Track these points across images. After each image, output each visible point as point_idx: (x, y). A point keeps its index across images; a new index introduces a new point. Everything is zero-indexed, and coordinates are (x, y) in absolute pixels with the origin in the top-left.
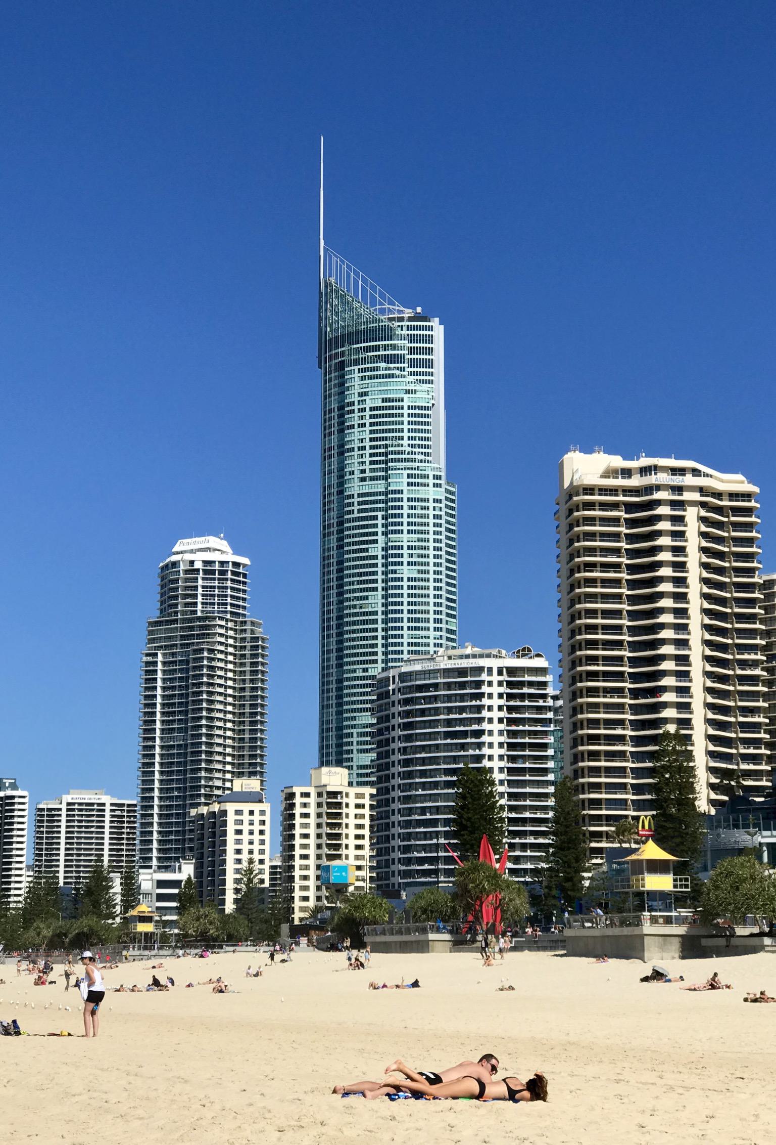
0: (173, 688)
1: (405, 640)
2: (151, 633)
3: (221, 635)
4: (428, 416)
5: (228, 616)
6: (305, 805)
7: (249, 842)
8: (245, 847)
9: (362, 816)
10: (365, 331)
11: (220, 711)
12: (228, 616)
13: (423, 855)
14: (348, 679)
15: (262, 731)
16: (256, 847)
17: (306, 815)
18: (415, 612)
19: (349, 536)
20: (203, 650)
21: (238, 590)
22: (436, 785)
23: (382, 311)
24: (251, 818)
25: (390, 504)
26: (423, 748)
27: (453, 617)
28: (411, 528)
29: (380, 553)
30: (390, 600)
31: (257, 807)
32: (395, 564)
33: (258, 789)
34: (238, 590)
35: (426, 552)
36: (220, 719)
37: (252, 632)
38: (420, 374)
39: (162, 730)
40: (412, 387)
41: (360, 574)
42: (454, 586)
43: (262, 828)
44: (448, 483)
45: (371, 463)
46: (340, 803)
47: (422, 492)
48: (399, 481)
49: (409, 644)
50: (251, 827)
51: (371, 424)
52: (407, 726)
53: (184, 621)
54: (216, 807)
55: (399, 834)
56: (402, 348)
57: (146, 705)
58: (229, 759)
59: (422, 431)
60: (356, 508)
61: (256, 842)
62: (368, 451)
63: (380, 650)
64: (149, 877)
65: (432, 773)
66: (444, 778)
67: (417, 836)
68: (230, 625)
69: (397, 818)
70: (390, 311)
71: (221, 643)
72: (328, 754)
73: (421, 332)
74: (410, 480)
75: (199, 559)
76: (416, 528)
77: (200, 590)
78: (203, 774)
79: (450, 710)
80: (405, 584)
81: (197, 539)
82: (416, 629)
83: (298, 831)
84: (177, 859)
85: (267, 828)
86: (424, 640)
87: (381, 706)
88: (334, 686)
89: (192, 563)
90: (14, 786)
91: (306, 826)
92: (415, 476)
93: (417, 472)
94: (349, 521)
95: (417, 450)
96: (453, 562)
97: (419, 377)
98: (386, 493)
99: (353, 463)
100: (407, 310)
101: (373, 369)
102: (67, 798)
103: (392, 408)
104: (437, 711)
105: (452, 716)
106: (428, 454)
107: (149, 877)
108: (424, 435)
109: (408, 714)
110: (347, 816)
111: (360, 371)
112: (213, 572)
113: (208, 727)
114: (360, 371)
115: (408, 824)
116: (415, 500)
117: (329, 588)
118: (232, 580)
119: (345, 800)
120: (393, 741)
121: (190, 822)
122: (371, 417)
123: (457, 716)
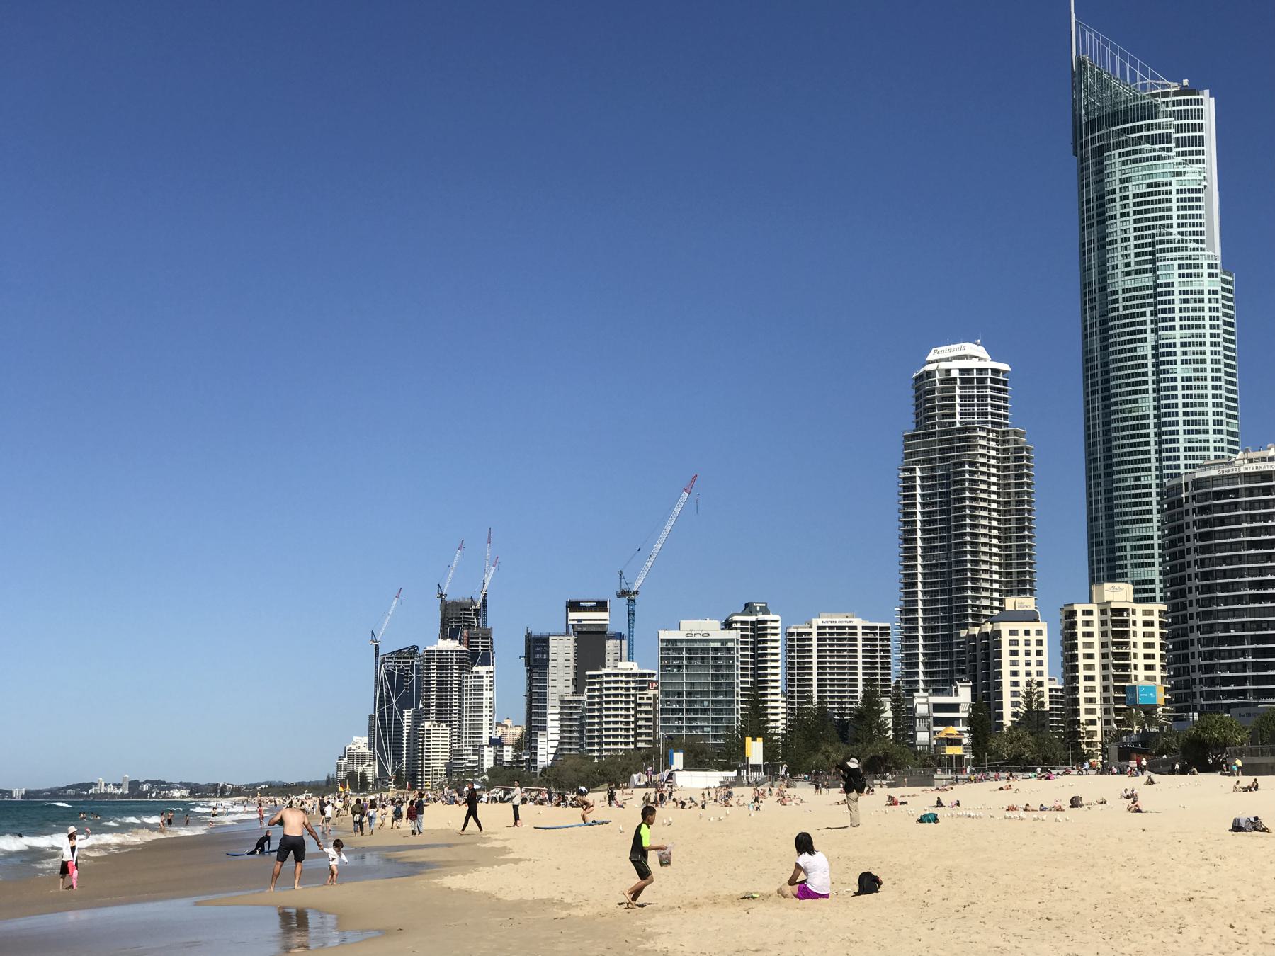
0: (933, 504)
1: (1182, 445)
2: (907, 447)
3: (983, 447)
4: (1200, 199)
5: (990, 426)
6: (1087, 623)
7: (1025, 662)
8: (1022, 669)
9: (1151, 634)
10: (1126, 111)
11: (984, 527)
12: (990, 426)
13: (1228, 674)
14: (1119, 489)
15: (1030, 546)
16: (1034, 669)
17: (1089, 634)
18: (1192, 414)
19: (1114, 336)
20: (964, 463)
21: (999, 399)
22: (1240, 599)
23: (1144, 87)
24: (1027, 638)
25: (1159, 298)
26: (1224, 560)
27: (1235, 417)
28: (1183, 323)
29: (1150, 352)
30: (1163, 402)
31: (1033, 627)
32: (1167, 363)
33: (1033, 608)
34: (999, 399)
35: (1202, 348)
36: (984, 535)
37: (1016, 442)
38: (1190, 153)
39: (924, 549)
40: (1180, 168)
41: (1129, 376)
42: (1234, 384)
43: (1039, 648)
44: (1224, 272)
45: (1137, 255)
46: (1127, 621)
47: (1195, 284)
48: (1170, 273)
49: (1186, 449)
50: (1028, 648)
51: (1135, 213)
52: (1204, 536)
53: (942, 433)
54: (988, 628)
55: (1200, 653)
56: (1168, 126)
57: (906, 523)
58: (996, 577)
59: (1194, 216)
60: (1121, 304)
61: (1034, 663)
62: (1132, 243)
63: (1153, 456)
64: (924, 700)
65: (1235, 586)
66: (1249, 592)
67: (1221, 655)
68: (991, 435)
69: (1196, 635)
70: (1153, 87)
71: (983, 455)
72: (1099, 570)
73: (1190, 107)
74: (1182, 271)
75: (955, 367)
76: (1190, 323)
77: (958, 400)
78: (969, 593)
79: (1253, 518)
80: (1180, 384)
81: (952, 346)
82: (1192, 432)
83: (1081, 651)
84: (952, 682)
85: (1044, 648)
86: (1203, 444)
87: (1173, 515)
88: (1102, 497)
89: (948, 371)
90: (765, 611)
91: (1089, 645)
92: (1187, 266)
93: (1188, 262)
94: (1114, 319)
95: (1188, 238)
96: (1233, 358)
97: (1188, 158)
98: (1155, 287)
99: (1117, 256)
100: (1172, 84)
101: (1136, 152)
102: (818, 622)
103: (1158, 193)
104: (1238, 519)
105: (1255, 524)
106: (1201, 242)
107: (924, 700)
108: (1195, 221)
109: (1205, 523)
110: (1135, 634)
111: (1121, 155)
112: (971, 381)
113: (972, 544)
114: (1121, 155)
115: (1210, 642)
116: (1188, 292)
117: (1093, 393)
118: (992, 388)
119: (1132, 618)
120: (1189, 553)
121: (958, 643)
122: (1135, 204)
123: (1262, 524)
